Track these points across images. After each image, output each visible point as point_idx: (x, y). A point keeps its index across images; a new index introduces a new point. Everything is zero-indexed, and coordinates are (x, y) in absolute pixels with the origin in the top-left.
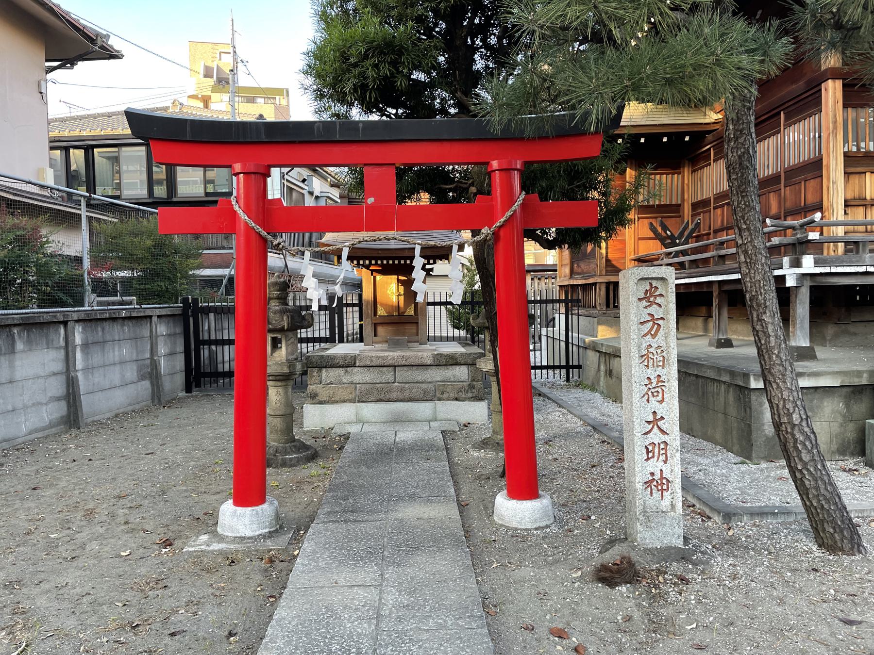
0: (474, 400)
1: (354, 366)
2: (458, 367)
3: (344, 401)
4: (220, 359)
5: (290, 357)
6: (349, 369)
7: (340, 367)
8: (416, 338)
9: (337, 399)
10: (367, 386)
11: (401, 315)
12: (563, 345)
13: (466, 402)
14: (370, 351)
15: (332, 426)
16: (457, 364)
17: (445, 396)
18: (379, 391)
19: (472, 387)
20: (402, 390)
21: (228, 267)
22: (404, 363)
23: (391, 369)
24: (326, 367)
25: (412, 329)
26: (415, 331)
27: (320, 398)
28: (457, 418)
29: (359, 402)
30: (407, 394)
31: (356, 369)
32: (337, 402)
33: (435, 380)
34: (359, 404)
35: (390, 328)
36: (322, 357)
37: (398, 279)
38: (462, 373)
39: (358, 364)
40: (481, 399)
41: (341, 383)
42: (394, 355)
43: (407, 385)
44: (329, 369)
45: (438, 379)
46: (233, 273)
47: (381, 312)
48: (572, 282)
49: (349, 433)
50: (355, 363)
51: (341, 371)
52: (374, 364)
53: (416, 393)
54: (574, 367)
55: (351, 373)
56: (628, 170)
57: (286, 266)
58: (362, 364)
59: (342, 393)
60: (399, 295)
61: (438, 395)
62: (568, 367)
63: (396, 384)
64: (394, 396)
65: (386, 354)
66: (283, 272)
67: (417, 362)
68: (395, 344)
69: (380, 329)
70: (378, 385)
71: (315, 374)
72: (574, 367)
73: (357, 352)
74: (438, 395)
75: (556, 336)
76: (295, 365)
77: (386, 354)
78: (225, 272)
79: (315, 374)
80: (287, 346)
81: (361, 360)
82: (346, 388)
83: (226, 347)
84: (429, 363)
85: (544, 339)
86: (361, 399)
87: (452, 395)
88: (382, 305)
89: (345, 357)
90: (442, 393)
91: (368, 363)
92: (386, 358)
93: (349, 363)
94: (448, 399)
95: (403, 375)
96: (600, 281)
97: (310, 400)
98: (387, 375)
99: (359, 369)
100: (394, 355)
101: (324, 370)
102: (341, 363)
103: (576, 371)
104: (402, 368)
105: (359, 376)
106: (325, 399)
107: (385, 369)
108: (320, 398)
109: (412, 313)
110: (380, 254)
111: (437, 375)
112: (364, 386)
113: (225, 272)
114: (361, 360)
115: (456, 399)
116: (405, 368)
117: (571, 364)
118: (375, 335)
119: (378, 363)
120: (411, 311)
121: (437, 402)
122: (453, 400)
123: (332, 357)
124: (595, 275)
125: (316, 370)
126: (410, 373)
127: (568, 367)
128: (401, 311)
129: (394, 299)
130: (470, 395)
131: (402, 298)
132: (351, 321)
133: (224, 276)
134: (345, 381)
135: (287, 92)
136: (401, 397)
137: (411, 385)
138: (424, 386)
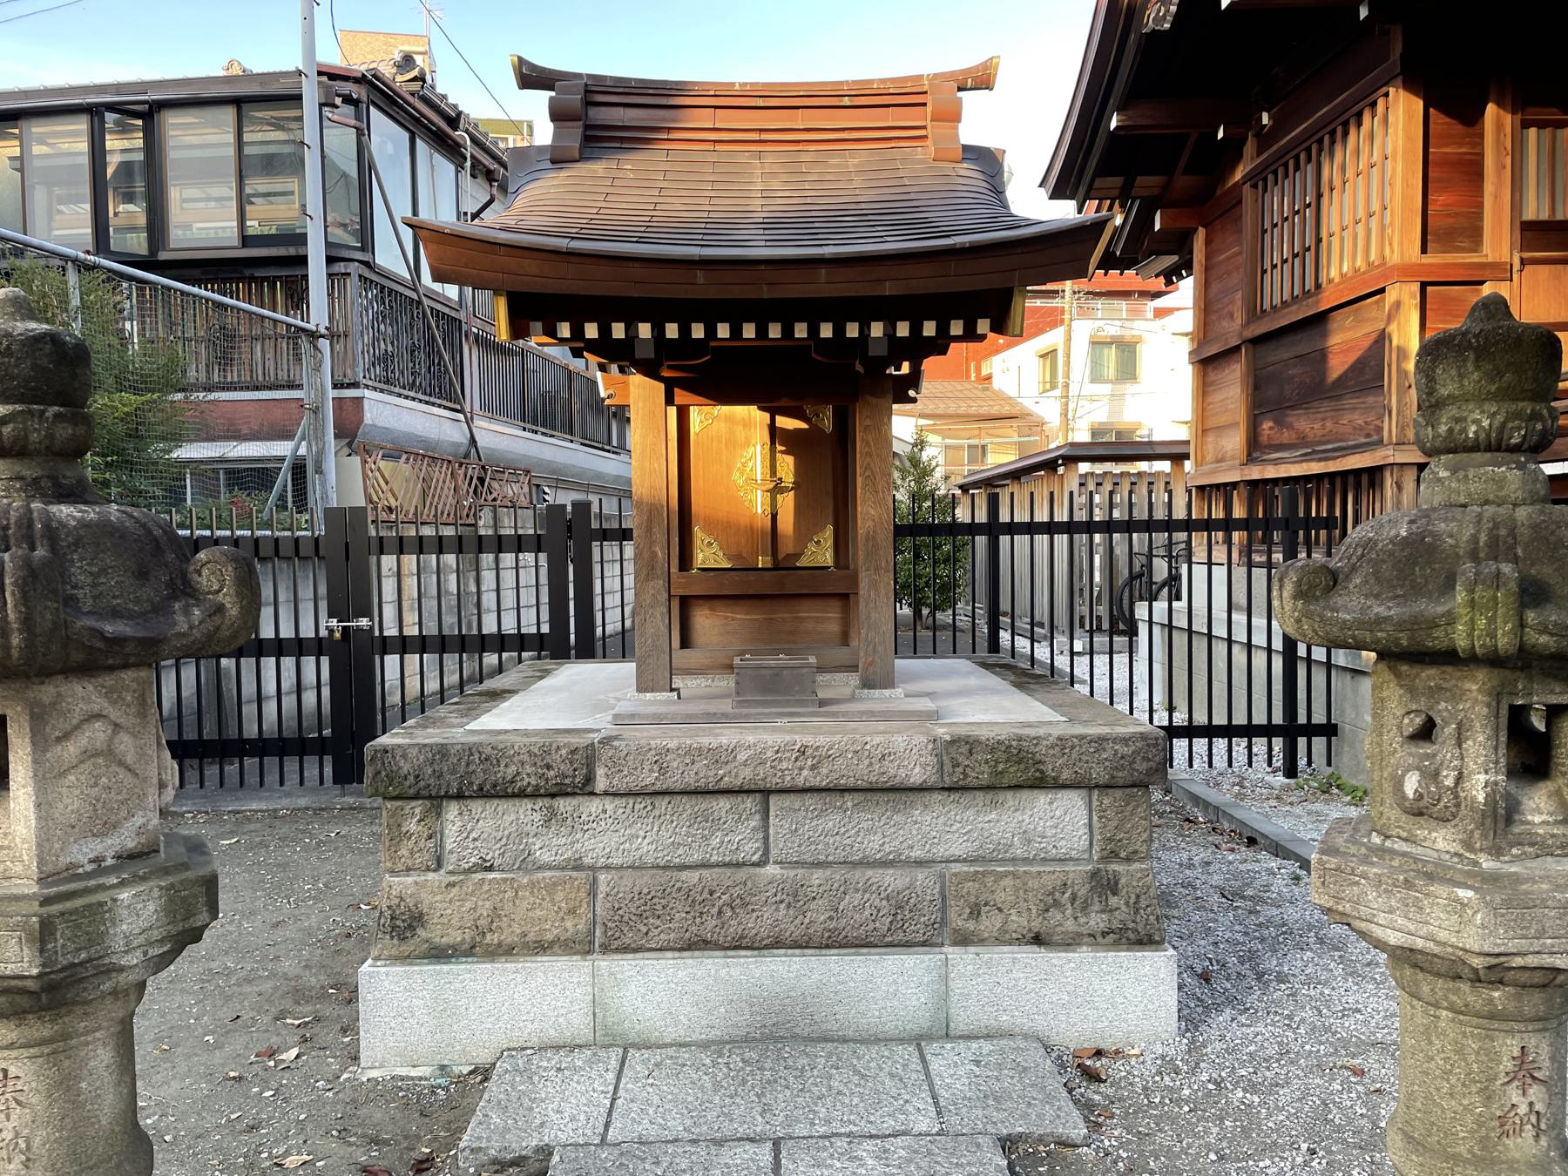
0: (1116, 945)
1: (585, 788)
2: (1042, 799)
3: (541, 948)
4: (249, 689)
5: (82, 853)
6: (563, 804)
7: (521, 794)
8: (842, 654)
9: (509, 935)
10: (644, 881)
11: (783, 565)
12: (1278, 663)
13: (1083, 955)
14: (657, 720)
15: (484, 1057)
16: (1041, 783)
17: (989, 923)
18: (697, 902)
19: (1103, 885)
20: (795, 897)
21: (286, 435)
22: (806, 777)
23: (749, 803)
24: (460, 796)
25: (827, 619)
26: (834, 627)
27: (435, 933)
28: (1041, 1024)
29: (606, 949)
30: (818, 915)
31: (594, 806)
32: (505, 951)
33: (941, 851)
34: (605, 964)
35: (740, 617)
36: (442, 751)
37: (772, 428)
38: (1061, 823)
39: (601, 784)
40: (1146, 941)
41: (526, 863)
42: (763, 740)
43: (817, 876)
44: (476, 806)
45: (957, 850)
46: (302, 451)
47: (706, 554)
48: (1255, 473)
49: (546, 1152)
50: (589, 779)
51: (525, 813)
52: (673, 782)
53: (859, 910)
54: (1311, 730)
55: (574, 824)
56: (1491, 109)
57: (473, 441)
58: (620, 783)
59: (533, 912)
60: (777, 490)
61: (958, 920)
62: (1291, 731)
63: (771, 870)
64: (760, 922)
65: (726, 736)
66: (467, 456)
67: (863, 772)
68: (768, 690)
69: (705, 622)
70: (692, 877)
71: (412, 826)
72: (1311, 730)
73: (602, 723)
74: (958, 920)
75: (1200, 625)
76: (98, 914)
77: (726, 736)
78: (282, 448)
79: (412, 826)
80: (45, 779)
81: (615, 765)
82: (553, 886)
83: (269, 663)
84: (917, 776)
85: (1143, 630)
86: (614, 935)
87: (1018, 922)
88: (710, 527)
89: (543, 748)
90: (975, 913)
91: (648, 779)
92: (719, 756)
93: (564, 777)
94: (1002, 939)
95: (800, 829)
96: (1400, 459)
97: (388, 944)
98: (735, 832)
99: (610, 804)
100: (763, 740)
101: (452, 810)
102: (529, 780)
103: (1319, 743)
104: (794, 801)
105: (608, 835)
106: (455, 937)
107: (723, 804)
108: (435, 933)
109: (827, 558)
110: (702, 287)
111: (953, 831)
112: (628, 880)
113: (282, 448)
114: (615, 765)
115: (1038, 940)
116: (810, 801)
117: (1302, 719)
118: (685, 643)
119: (690, 780)
120: (821, 552)
121: (953, 952)
122: (1020, 941)
123: (486, 754)
124: (1380, 442)
125: (418, 807)
126: (832, 821)
127: (1291, 731)
128: (787, 547)
129: (759, 503)
130: (1097, 921)
131: (787, 502)
132: (617, 583)
133: (282, 459)
134: (546, 857)
135: (530, 127)
136: (792, 930)
137: (838, 875)
138: (893, 880)
